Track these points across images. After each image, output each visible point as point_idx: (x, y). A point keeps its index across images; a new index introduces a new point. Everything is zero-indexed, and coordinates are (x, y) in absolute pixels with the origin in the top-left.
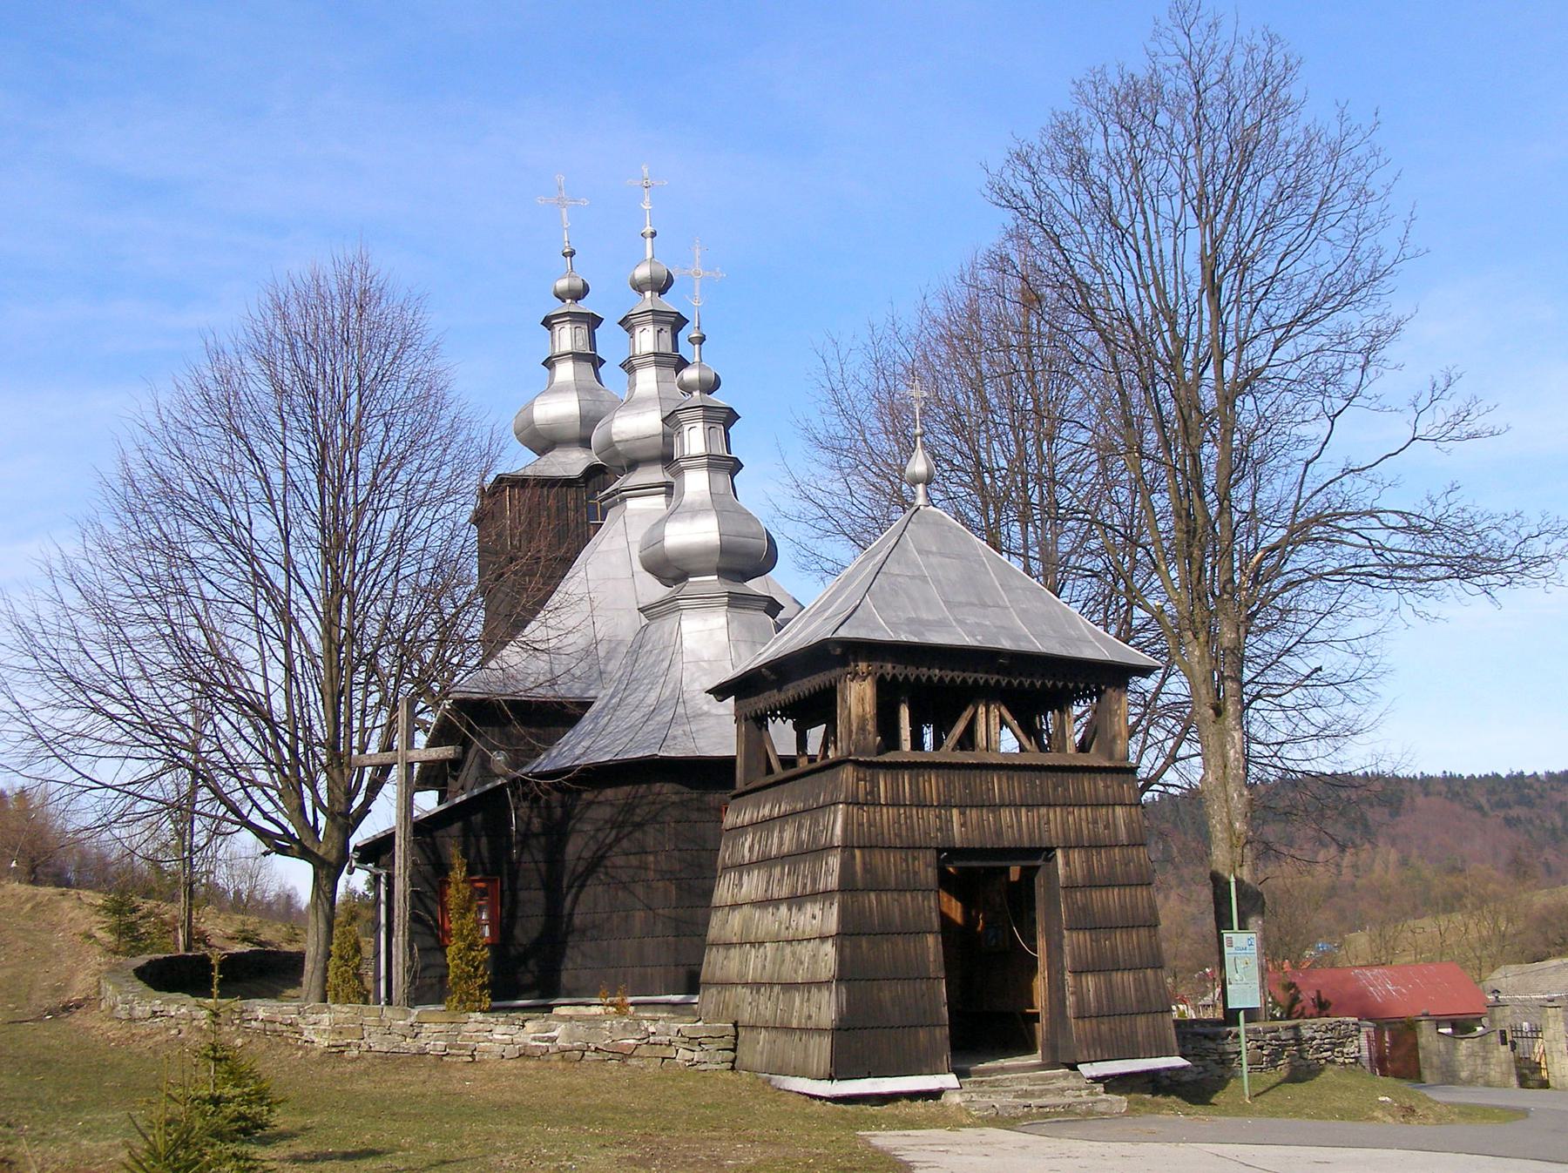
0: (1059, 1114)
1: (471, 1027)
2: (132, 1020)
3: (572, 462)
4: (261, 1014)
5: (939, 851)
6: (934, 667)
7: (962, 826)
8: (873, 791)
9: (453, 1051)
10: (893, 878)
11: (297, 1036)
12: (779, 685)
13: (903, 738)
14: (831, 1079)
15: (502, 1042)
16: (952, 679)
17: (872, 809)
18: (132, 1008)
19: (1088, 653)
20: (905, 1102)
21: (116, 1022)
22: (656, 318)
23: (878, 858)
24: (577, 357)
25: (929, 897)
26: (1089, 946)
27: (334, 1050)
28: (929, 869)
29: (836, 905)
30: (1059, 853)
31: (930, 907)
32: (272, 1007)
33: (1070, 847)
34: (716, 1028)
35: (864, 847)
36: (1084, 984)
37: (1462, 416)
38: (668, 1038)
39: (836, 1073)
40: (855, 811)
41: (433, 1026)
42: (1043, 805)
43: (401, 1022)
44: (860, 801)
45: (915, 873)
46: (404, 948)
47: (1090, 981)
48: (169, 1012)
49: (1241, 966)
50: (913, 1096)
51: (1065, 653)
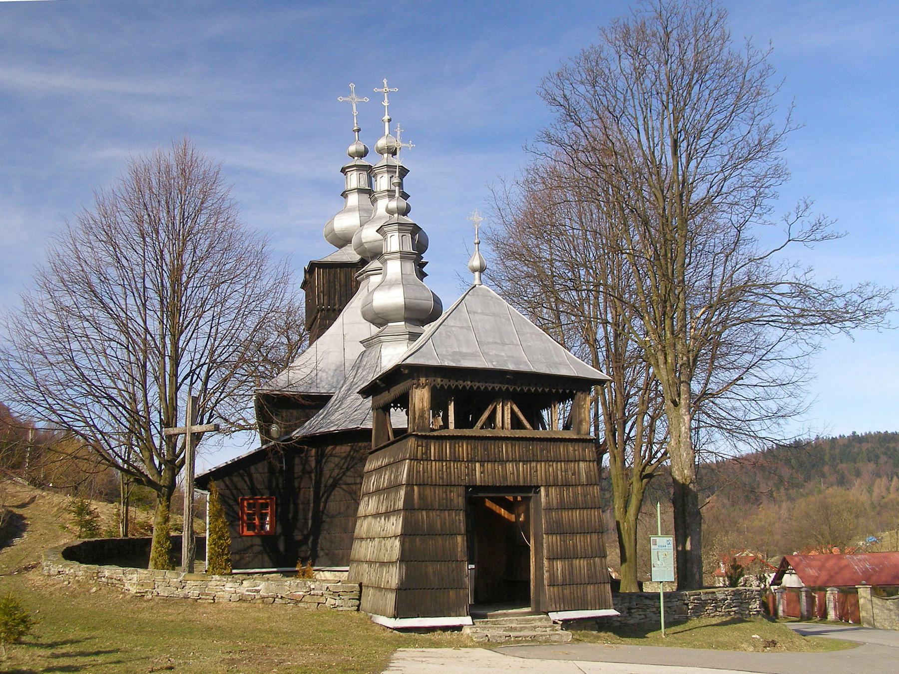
0: (527, 641)
1: (213, 583)
2: (49, 576)
3: (350, 255)
4: (107, 574)
5: (467, 487)
6: (467, 380)
7: (481, 473)
8: (427, 452)
9: (203, 597)
10: (437, 503)
11: (122, 586)
12: (388, 388)
13: (450, 421)
14: (395, 617)
15: (230, 592)
16: (479, 388)
17: (426, 463)
18: (50, 569)
19: (563, 372)
20: (439, 632)
21: (42, 577)
22: (389, 169)
23: (428, 491)
24: (360, 191)
25: (459, 514)
26: (559, 544)
27: (139, 595)
28: (460, 498)
29: (401, 518)
30: (542, 489)
31: (459, 520)
32: (111, 570)
33: (550, 486)
34: (348, 586)
35: (420, 485)
36: (555, 566)
37: (817, 226)
38: (321, 592)
39: (397, 615)
40: (415, 464)
41: (192, 582)
42: (533, 461)
43: (175, 580)
44: (419, 458)
45: (451, 500)
46: (188, 538)
47: (559, 565)
48: (65, 572)
49: (661, 557)
50: (445, 629)
51: (548, 372)
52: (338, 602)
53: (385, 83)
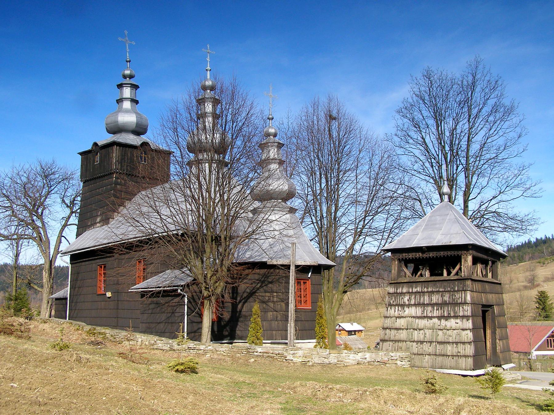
52: (403, 363)
53: (208, 47)
